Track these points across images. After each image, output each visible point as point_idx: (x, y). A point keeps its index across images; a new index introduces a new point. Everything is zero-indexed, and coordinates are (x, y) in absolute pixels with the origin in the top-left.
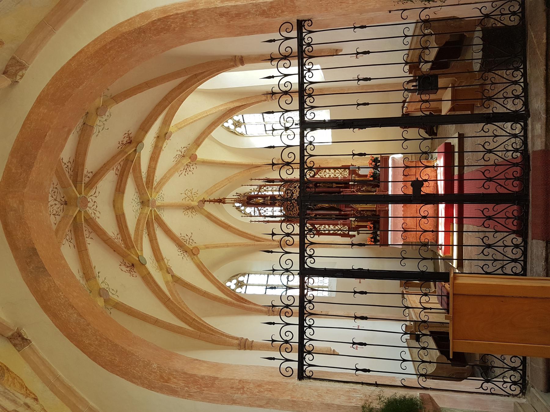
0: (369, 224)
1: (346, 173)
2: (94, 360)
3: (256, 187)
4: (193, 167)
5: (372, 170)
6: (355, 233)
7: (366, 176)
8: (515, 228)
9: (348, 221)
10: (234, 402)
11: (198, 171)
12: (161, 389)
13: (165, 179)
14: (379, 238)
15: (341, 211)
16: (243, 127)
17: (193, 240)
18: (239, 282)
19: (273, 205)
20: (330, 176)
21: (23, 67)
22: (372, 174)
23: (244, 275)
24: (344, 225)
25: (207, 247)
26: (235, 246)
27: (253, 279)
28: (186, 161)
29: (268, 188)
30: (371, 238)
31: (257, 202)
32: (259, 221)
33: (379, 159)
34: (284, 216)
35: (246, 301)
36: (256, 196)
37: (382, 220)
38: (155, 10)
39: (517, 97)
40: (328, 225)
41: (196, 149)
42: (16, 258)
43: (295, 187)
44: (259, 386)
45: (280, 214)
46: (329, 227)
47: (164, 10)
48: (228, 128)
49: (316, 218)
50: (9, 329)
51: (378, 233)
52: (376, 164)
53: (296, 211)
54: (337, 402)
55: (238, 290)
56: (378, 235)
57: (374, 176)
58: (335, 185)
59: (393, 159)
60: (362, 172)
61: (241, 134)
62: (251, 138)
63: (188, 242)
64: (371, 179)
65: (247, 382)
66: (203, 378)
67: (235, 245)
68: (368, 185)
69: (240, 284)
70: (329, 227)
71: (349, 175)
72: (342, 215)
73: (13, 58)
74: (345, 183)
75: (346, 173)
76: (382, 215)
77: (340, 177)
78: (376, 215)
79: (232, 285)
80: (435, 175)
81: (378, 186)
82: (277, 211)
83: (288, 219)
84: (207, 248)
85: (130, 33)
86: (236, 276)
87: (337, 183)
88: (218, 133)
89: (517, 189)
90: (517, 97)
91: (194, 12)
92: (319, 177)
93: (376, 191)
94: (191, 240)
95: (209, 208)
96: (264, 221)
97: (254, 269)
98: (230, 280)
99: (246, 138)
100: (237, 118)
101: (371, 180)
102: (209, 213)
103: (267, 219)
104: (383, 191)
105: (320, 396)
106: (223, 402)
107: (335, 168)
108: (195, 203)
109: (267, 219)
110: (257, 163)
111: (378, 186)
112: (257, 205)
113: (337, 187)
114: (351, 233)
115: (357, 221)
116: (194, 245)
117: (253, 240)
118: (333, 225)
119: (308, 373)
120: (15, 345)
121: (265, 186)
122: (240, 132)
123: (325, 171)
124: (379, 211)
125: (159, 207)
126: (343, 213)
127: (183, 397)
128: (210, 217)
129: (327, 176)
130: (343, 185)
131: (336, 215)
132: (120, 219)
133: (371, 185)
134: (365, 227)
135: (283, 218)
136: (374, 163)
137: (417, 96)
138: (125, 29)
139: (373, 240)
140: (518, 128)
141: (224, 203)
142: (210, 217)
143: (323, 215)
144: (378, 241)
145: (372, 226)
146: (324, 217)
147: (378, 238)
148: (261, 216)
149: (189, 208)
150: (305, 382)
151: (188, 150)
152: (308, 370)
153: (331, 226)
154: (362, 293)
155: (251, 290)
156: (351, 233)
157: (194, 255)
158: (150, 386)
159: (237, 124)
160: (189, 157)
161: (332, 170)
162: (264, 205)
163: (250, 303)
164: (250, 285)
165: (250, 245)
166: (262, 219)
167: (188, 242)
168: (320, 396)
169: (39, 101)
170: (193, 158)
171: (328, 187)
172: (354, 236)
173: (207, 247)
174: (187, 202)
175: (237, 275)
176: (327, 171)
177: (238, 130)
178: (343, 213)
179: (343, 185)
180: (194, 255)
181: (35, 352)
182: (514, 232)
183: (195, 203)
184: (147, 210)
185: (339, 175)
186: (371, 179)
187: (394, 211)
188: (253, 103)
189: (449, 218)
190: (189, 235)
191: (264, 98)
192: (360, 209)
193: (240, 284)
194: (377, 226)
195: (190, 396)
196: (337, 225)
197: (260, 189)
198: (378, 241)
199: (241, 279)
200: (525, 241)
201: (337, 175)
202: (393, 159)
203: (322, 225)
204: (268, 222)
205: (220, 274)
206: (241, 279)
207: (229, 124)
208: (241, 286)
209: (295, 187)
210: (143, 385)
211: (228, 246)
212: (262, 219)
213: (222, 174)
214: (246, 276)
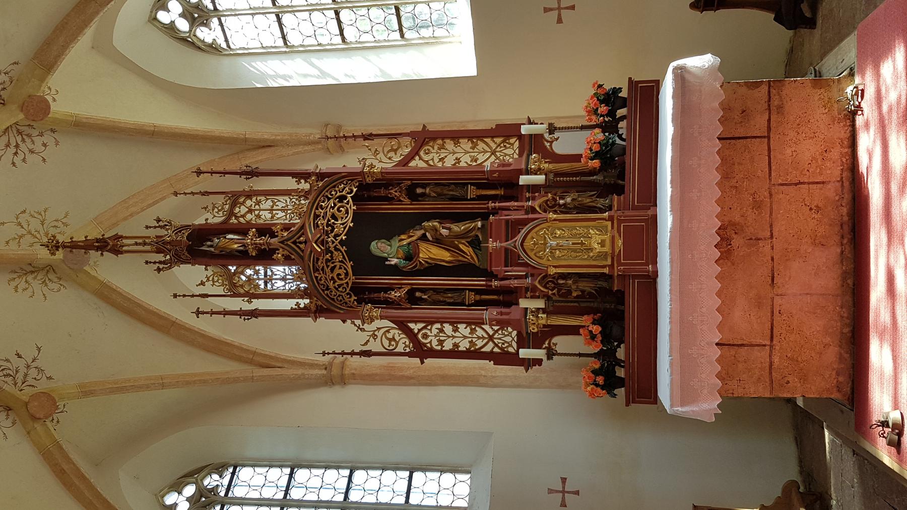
0: (584, 320)
3: (220, 200)
4: (45, 139)
5: (599, 135)
6: (539, 353)
7: (577, 158)
9: (514, 313)
15: (490, 275)
17: (40, 370)
20: (458, 160)
22: (596, 148)
23: (219, 469)
26: (188, 383)
29: (258, 203)
30: (596, 372)
31: (223, 249)
32: (225, 313)
33: (624, 94)
36: (221, 230)
40: (451, 323)
41: (42, 80)
43: (342, 198)
46: (456, 330)
48: (171, 28)
49: (412, 299)
51: (621, 353)
52: (611, 114)
53: (343, 273)
56: (618, 363)
57: (607, 154)
58: (472, 192)
59: (681, 75)
60: (564, 145)
61: (213, 49)
62: (244, 62)
63: (20, 376)
64: (596, 163)
70: (456, 330)
71: (520, 155)
72: (496, 291)
74: (505, 184)
75: (511, 153)
78: (609, 292)
80: (844, 134)
81: (620, 191)
86: (194, 474)
87: (479, 186)
92: (422, 164)
93: (610, 208)
94: (33, 373)
96: (241, 313)
97: (251, 452)
98: (178, 487)
99: (226, 61)
101: (592, 172)
102: (105, 285)
104: (635, 208)
107: (476, 136)
110: (258, 136)
111: (620, 191)
113: (480, 198)
114: (524, 353)
115: (544, 311)
116: (43, 385)
117: (250, 362)
118: (469, 324)
121: (249, 197)
122: (209, 40)
123: (442, 147)
124: (623, 277)
126: (495, 283)
128: (107, 295)
129: (449, 162)
130: (500, 192)
131: (478, 292)
134: (573, 331)
135: (304, 302)
136: (603, 109)
139: (600, 380)
141: (117, 251)
142: (107, 295)
143: (436, 291)
144: (621, 382)
145: (596, 329)
146: (439, 298)
147: (621, 373)
153: (461, 327)
156: (524, 353)
157: (34, 418)
161: (463, 141)
162: (243, 257)
165: (236, 380)
167: (20, 376)
170: (37, 110)
171: (453, 199)
172: (538, 362)
173: (86, 392)
175: (199, 470)
176: (450, 145)
177: (205, 34)
178: (495, 283)
179: (500, 192)
180: (34, 418)
185: (485, 158)
186: (596, 163)
190: (29, 353)
192: (552, 271)
194: (616, 331)
196: (480, 323)
197: (234, 205)
201: (481, 158)
202: (681, 75)
203: (432, 323)
204: (255, 314)
206: (211, 481)
209: (342, 198)
211: (163, 386)
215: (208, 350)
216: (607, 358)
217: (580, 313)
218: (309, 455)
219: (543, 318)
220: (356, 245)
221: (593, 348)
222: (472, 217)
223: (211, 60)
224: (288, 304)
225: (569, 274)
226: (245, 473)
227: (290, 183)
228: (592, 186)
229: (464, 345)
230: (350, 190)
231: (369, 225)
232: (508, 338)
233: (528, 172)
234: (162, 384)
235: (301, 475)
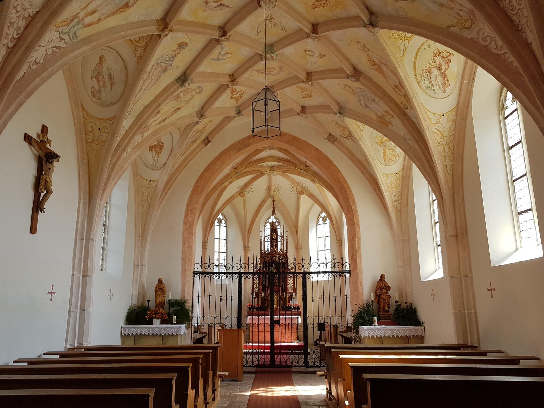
1: (57, 356)
2: (199, 178)
5: (292, 306)
6: (254, 296)
8: (260, 363)
10: (183, 244)
11: (294, 195)
12: (187, 210)
13: (288, 178)
14: (252, 310)
15: (268, 287)
16: (323, 222)
18: (221, 220)
19: (272, 246)
21: (333, 143)
23: (226, 223)
24: (259, 289)
25: (244, 201)
27: (223, 229)
28: (299, 189)
34: (265, 252)
35: (211, 228)
37: (262, 312)
38: (356, 207)
39: (314, 363)
42: (244, 138)
44: (190, 255)
45: (266, 250)
47: (356, 211)
50: (212, 139)
54: (186, 289)
55: (216, 221)
57: (289, 308)
58: (283, 283)
61: (318, 221)
62: (315, 229)
65: (192, 249)
66: (192, 229)
67: (245, 218)
68: (283, 304)
69: (220, 222)
73: (337, 139)
74: (285, 290)
76: (266, 312)
77: (289, 286)
79: (220, 216)
81: (283, 310)
82: (268, 246)
83: (263, 255)
84: (244, 202)
85: (347, 194)
86: (225, 218)
88: (317, 209)
89: (276, 363)
90: (314, 363)
91: (354, 225)
95: (269, 201)
97: (229, 231)
100: (328, 221)
102: (266, 201)
103: (263, 241)
105: (188, 281)
106: (183, 239)
108: (272, 193)
109: (263, 241)
111: (283, 310)
112: (271, 235)
114: (254, 293)
116: (246, 193)
117: (249, 229)
119: (196, 276)
120: (204, 140)
125: (270, 175)
127: (184, 221)
132: (263, 160)
133: (284, 305)
134: (258, 302)
137: (316, 322)
138: (348, 193)
140: (302, 363)
142: (264, 202)
144: (250, 310)
148: (265, 237)
149: (269, 189)
150: (192, 274)
151: (307, 190)
152: (196, 276)
154: (221, 299)
155: (216, 228)
156: (254, 293)
158: (188, 205)
159: (324, 219)
160: (302, 191)
163: (210, 230)
164: (220, 228)
166: (263, 238)
168: (188, 281)
169: (317, 150)
170: (301, 193)
173: (244, 201)
174: (273, 189)
177: (321, 219)
181: (202, 149)
182: (259, 362)
183: (272, 193)
184: (268, 170)
187: (267, 318)
188: (335, 231)
189: (264, 348)
191: (338, 239)
193: (220, 222)
195: (185, 223)
198: (250, 310)
199: (223, 221)
200: (255, 366)
204: (261, 242)
205: (228, 210)
206: (223, 221)
207: (324, 215)
208: (218, 222)
210: (189, 201)
212: (263, 238)
213: (291, 209)
214: (225, 225)
215: (252, 220)
216: (254, 308)
217: (262, 303)
218: (229, 243)
219: (260, 297)
220: (274, 262)
221: (256, 306)
222: (279, 283)
223: (316, 221)
224: (263, 249)
225: (7, 110)
226: (225, 228)
227: (285, 249)
228: (284, 305)
229: (255, 282)
230: (283, 261)
231: (277, 264)
232: (256, 290)
233: (286, 294)
234: (245, 213)
235: (225, 241)
